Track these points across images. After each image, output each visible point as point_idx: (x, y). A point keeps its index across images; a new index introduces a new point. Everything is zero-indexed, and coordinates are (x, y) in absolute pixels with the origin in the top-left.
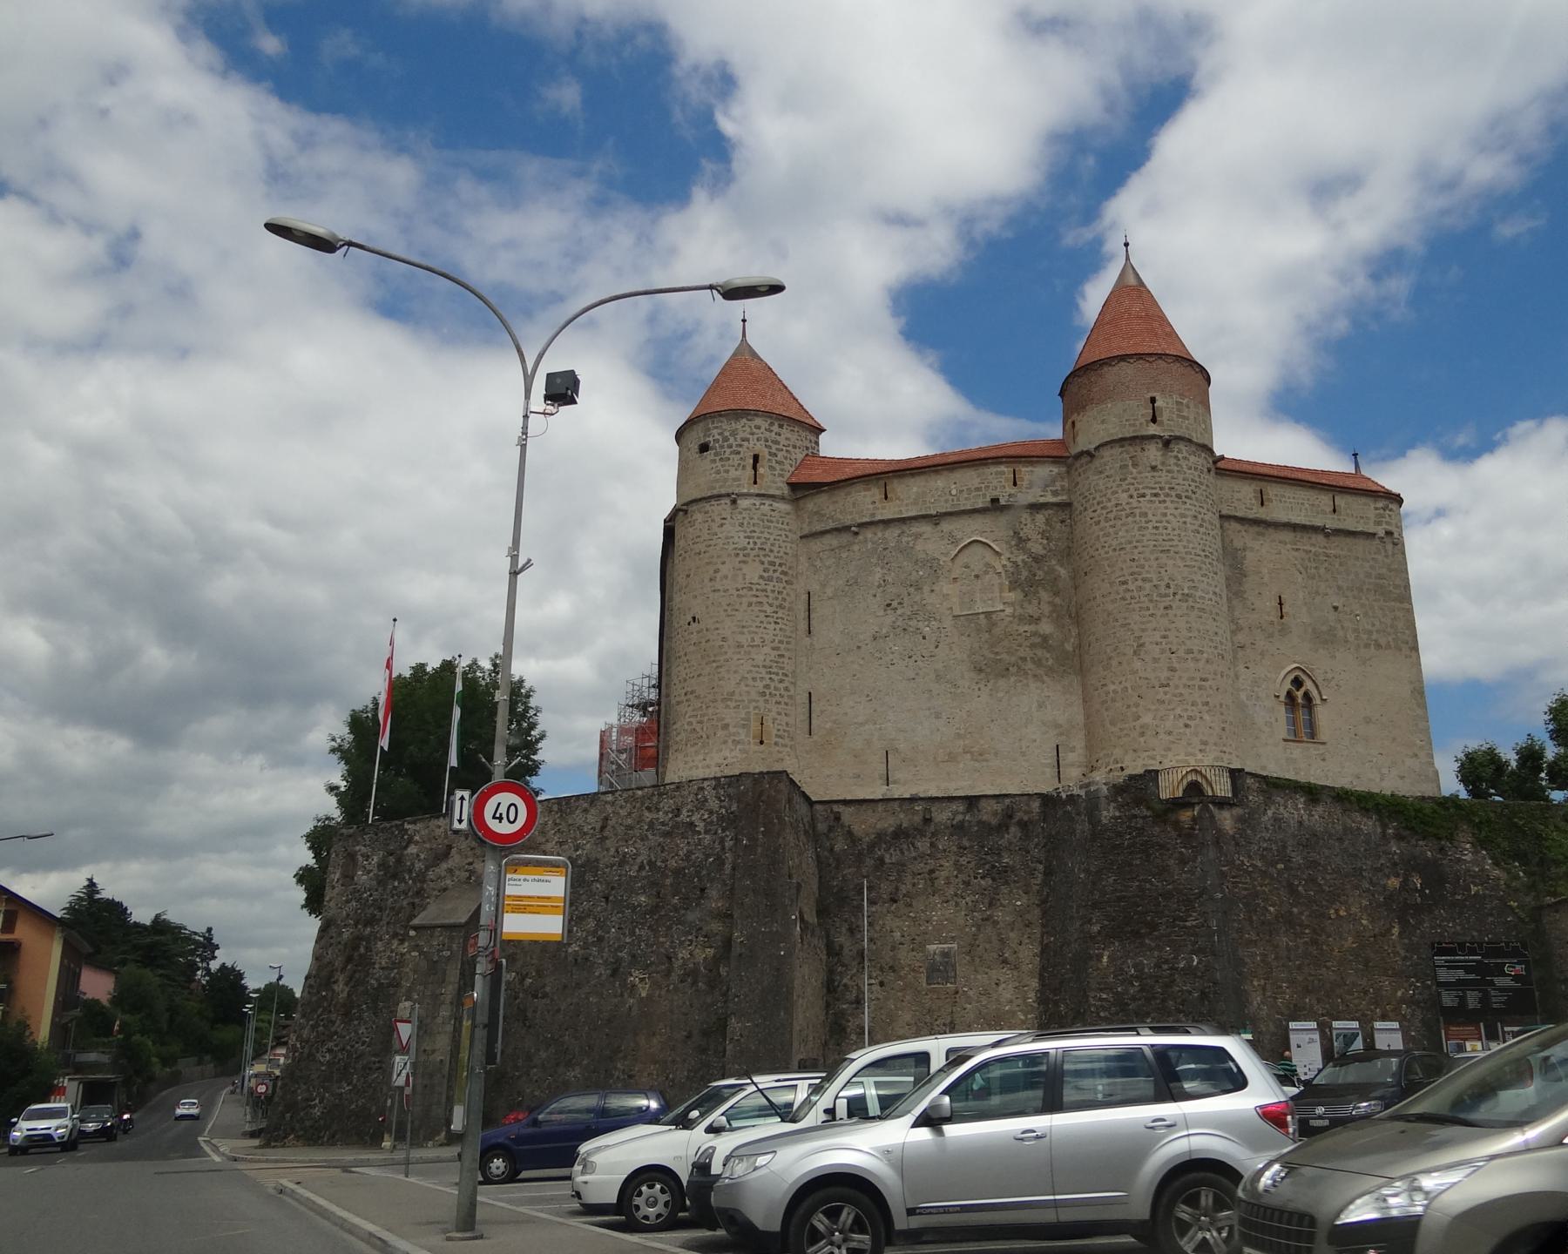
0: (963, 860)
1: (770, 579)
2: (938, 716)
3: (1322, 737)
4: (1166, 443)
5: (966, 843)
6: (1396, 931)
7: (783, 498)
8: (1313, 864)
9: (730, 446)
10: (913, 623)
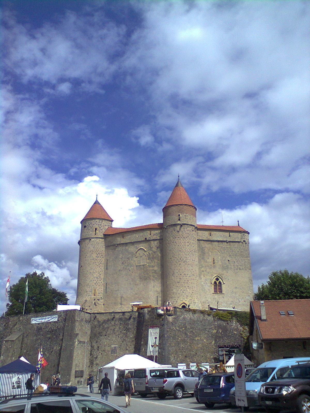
0: (121, 327)
1: (98, 257)
2: (132, 289)
3: (223, 292)
4: (181, 226)
5: (121, 323)
6: (213, 342)
7: (102, 238)
8: (193, 328)
9: (90, 226)
10: (128, 267)
